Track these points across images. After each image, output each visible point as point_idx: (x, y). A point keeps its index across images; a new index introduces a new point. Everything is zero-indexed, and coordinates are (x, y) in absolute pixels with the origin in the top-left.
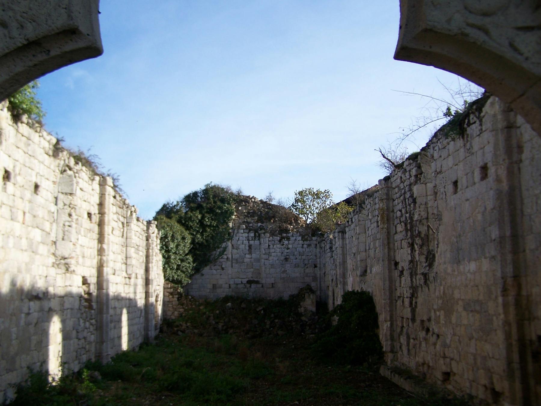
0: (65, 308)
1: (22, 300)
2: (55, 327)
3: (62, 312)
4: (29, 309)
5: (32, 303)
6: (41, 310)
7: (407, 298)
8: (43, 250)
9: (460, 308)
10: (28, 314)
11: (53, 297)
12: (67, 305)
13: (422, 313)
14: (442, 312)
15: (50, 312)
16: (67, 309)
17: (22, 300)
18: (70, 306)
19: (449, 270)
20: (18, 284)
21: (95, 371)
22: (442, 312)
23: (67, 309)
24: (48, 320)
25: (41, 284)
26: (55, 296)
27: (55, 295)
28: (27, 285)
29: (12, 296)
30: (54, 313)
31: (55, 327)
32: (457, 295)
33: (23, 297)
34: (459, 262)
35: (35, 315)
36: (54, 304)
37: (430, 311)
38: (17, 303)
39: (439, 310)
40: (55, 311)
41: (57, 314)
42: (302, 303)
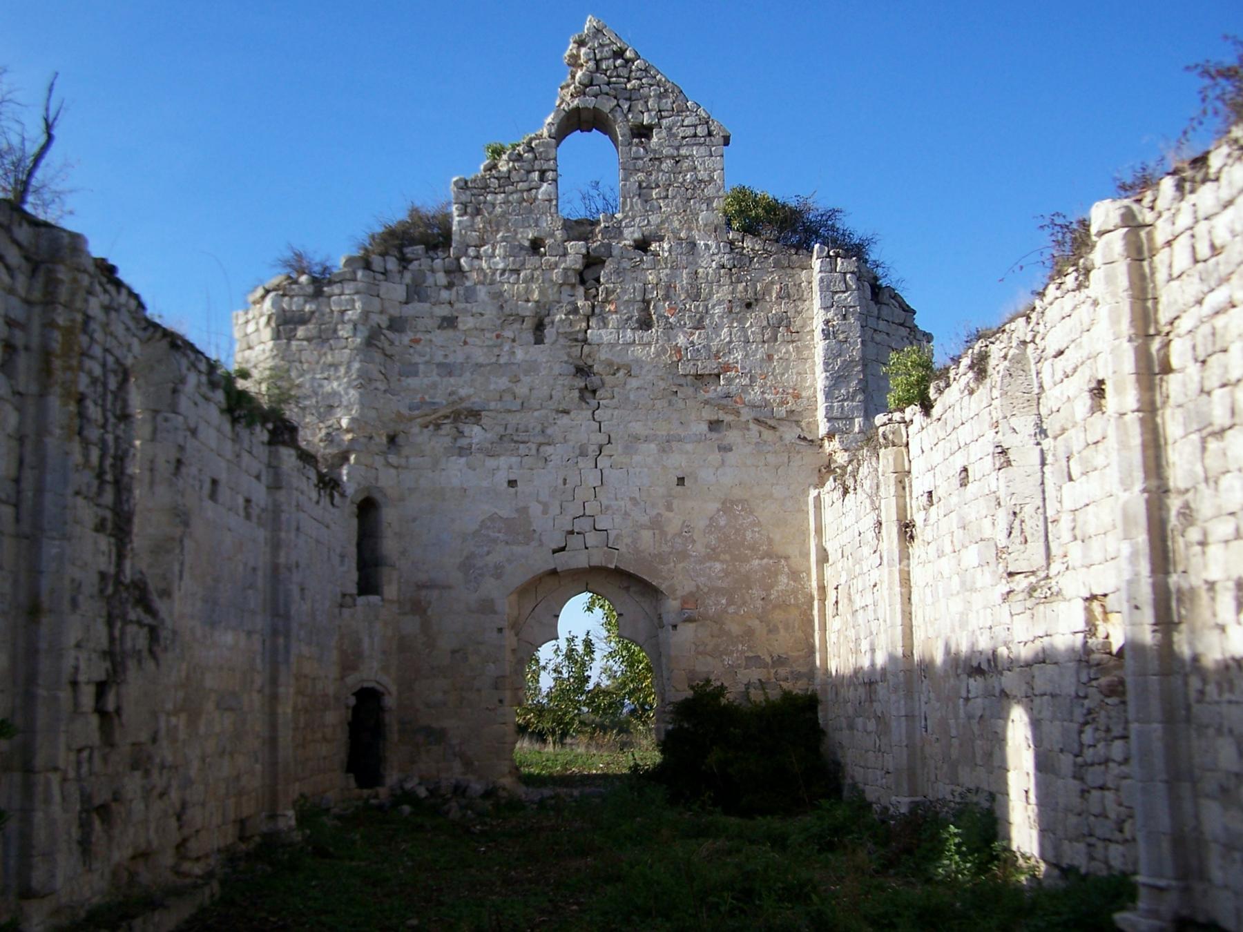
0: (1036, 692)
1: (958, 676)
2: (1018, 730)
3: (1029, 700)
4: (968, 691)
5: (971, 681)
6: (988, 694)
7: (88, 683)
8: (984, 578)
9: (210, 706)
10: (967, 699)
11: (1006, 666)
12: (1040, 685)
13: (134, 727)
14: (183, 717)
15: (1003, 698)
16: (1043, 695)
17: (958, 676)
18: (1049, 689)
19: (199, 633)
20: (953, 650)
21: (666, 745)
22: (183, 717)
23: (1043, 695)
24: (1004, 716)
25: (984, 644)
26: (1012, 663)
27: (1011, 661)
28: (964, 648)
29: (946, 671)
30: (1013, 702)
31: (1018, 730)
32: (210, 682)
33: (959, 671)
34: (213, 625)
35: (978, 705)
36: (1009, 680)
37: (154, 715)
38: (952, 680)
39: (176, 712)
40: (1015, 697)
41: (1018, 702)
42: (1083, 871)
